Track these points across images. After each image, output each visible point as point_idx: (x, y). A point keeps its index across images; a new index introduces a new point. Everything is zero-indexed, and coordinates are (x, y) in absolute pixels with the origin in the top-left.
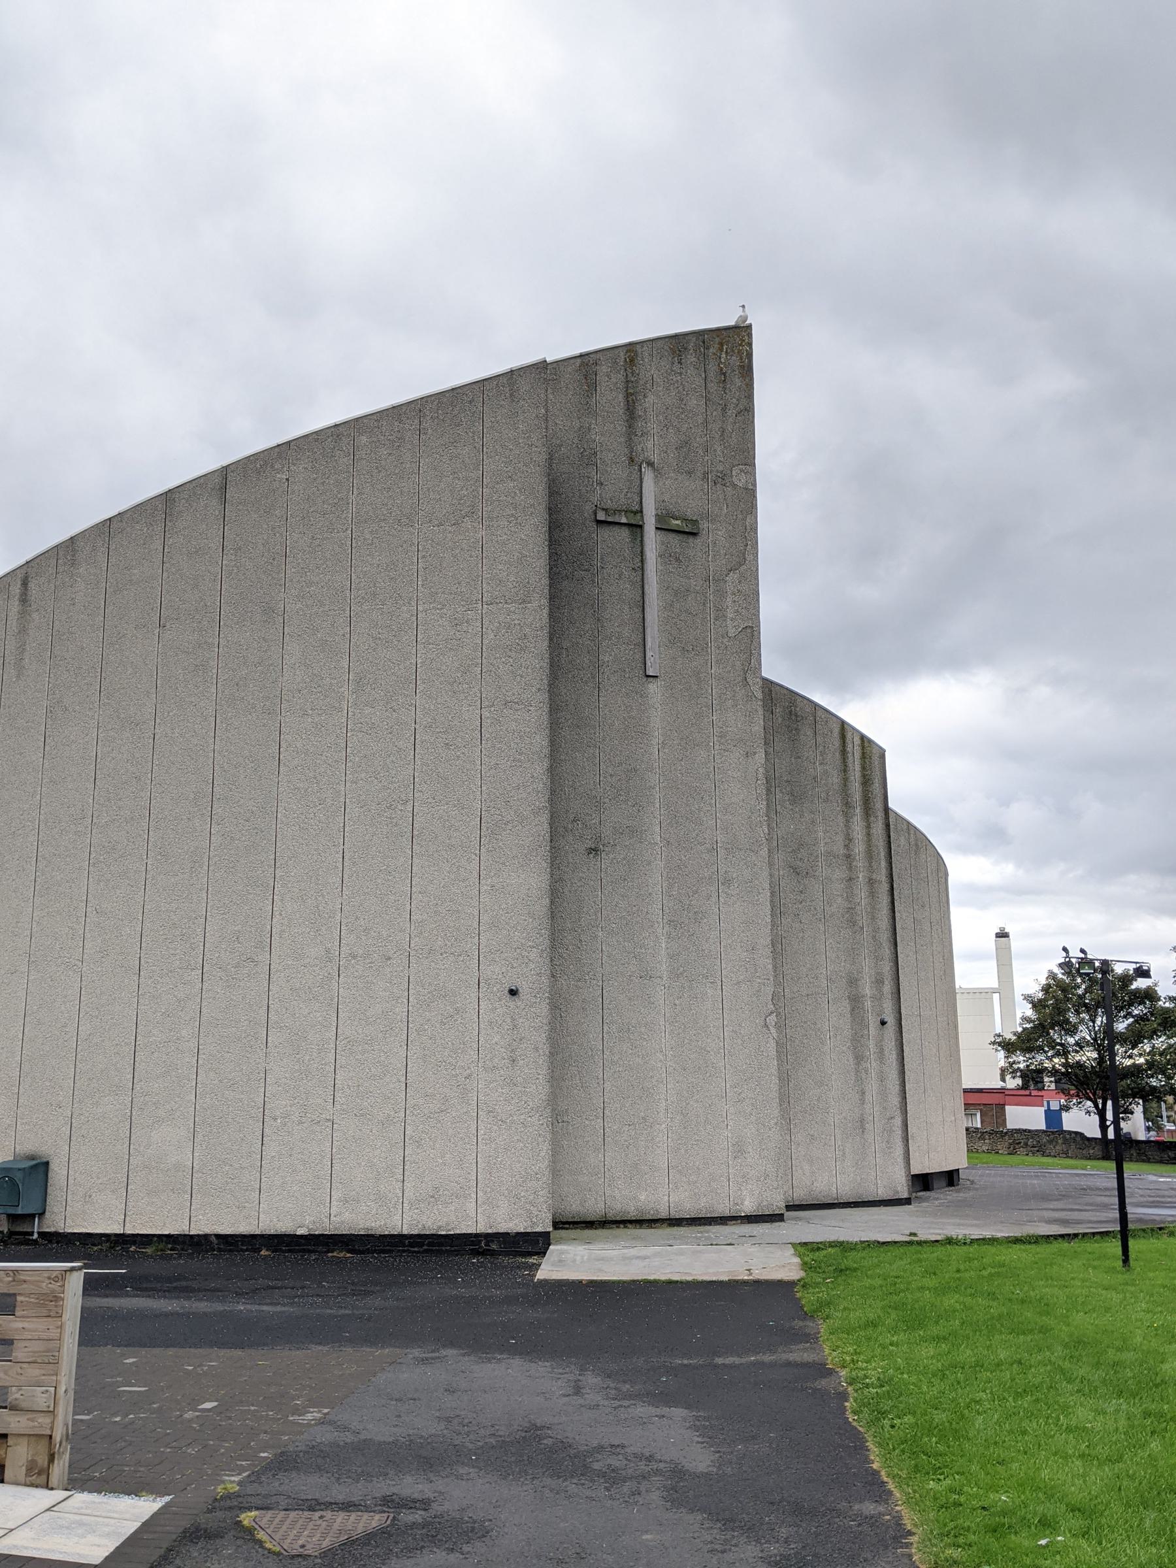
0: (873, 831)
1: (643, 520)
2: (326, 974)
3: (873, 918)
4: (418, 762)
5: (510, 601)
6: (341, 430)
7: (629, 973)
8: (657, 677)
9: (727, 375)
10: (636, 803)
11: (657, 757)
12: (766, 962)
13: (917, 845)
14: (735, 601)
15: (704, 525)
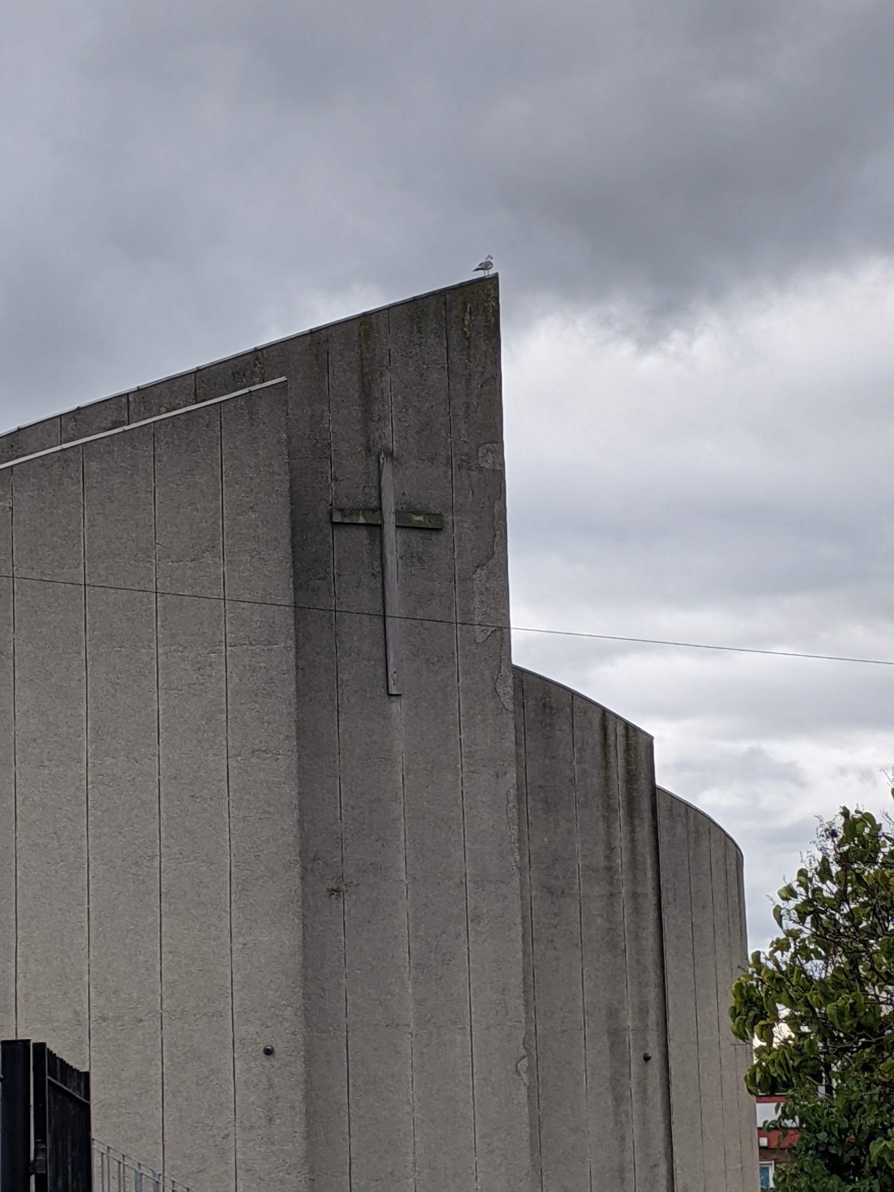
0: (638, 836)
1: (382, 520)
2: (76, 1038)
3: (637, 938)
4: (163, 816)
5: (254, 642)
6: (68, 454)
7: (375, 1022)
8: (400, 695)
9: (471, 339)
10: (380, 838)
11: (402, 785)
12: (517, 1003)
13: (697, 831)
14: (483, 602)
15: (448, 518)
